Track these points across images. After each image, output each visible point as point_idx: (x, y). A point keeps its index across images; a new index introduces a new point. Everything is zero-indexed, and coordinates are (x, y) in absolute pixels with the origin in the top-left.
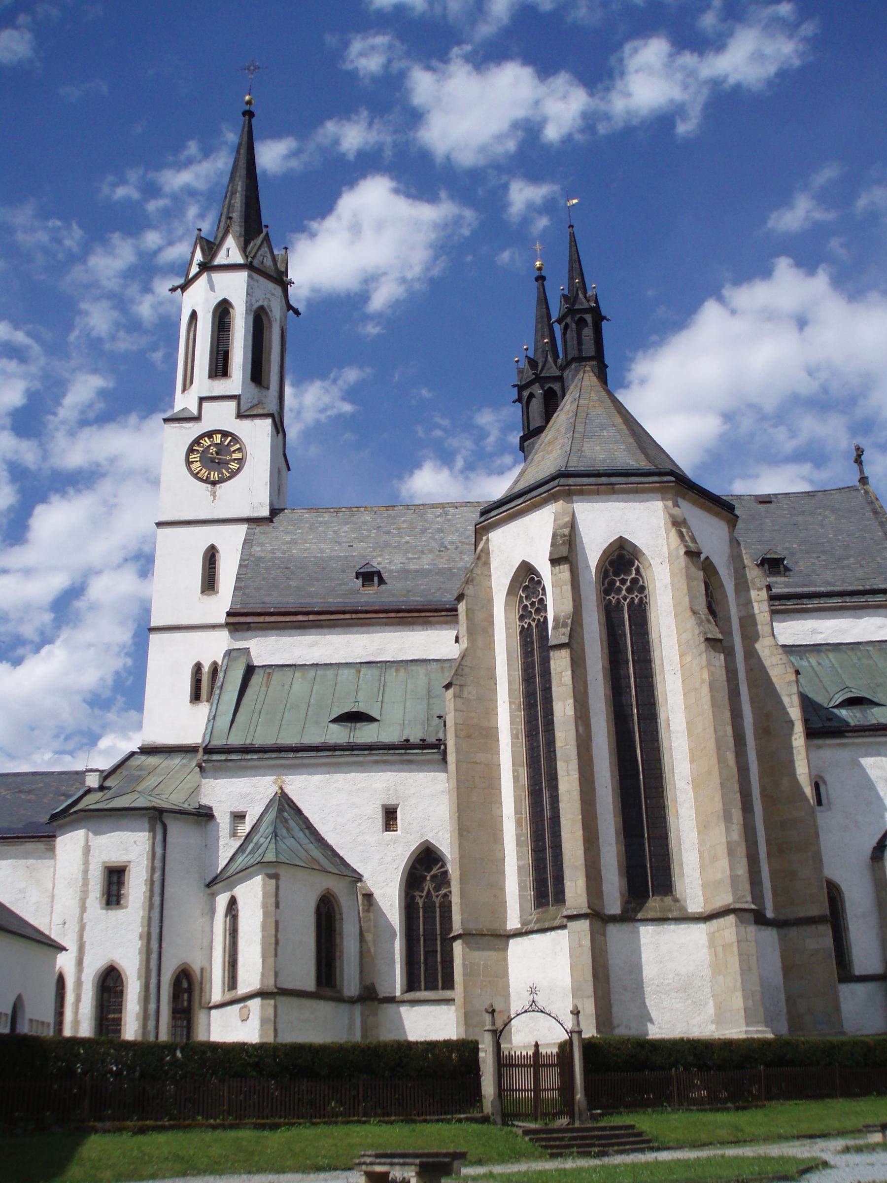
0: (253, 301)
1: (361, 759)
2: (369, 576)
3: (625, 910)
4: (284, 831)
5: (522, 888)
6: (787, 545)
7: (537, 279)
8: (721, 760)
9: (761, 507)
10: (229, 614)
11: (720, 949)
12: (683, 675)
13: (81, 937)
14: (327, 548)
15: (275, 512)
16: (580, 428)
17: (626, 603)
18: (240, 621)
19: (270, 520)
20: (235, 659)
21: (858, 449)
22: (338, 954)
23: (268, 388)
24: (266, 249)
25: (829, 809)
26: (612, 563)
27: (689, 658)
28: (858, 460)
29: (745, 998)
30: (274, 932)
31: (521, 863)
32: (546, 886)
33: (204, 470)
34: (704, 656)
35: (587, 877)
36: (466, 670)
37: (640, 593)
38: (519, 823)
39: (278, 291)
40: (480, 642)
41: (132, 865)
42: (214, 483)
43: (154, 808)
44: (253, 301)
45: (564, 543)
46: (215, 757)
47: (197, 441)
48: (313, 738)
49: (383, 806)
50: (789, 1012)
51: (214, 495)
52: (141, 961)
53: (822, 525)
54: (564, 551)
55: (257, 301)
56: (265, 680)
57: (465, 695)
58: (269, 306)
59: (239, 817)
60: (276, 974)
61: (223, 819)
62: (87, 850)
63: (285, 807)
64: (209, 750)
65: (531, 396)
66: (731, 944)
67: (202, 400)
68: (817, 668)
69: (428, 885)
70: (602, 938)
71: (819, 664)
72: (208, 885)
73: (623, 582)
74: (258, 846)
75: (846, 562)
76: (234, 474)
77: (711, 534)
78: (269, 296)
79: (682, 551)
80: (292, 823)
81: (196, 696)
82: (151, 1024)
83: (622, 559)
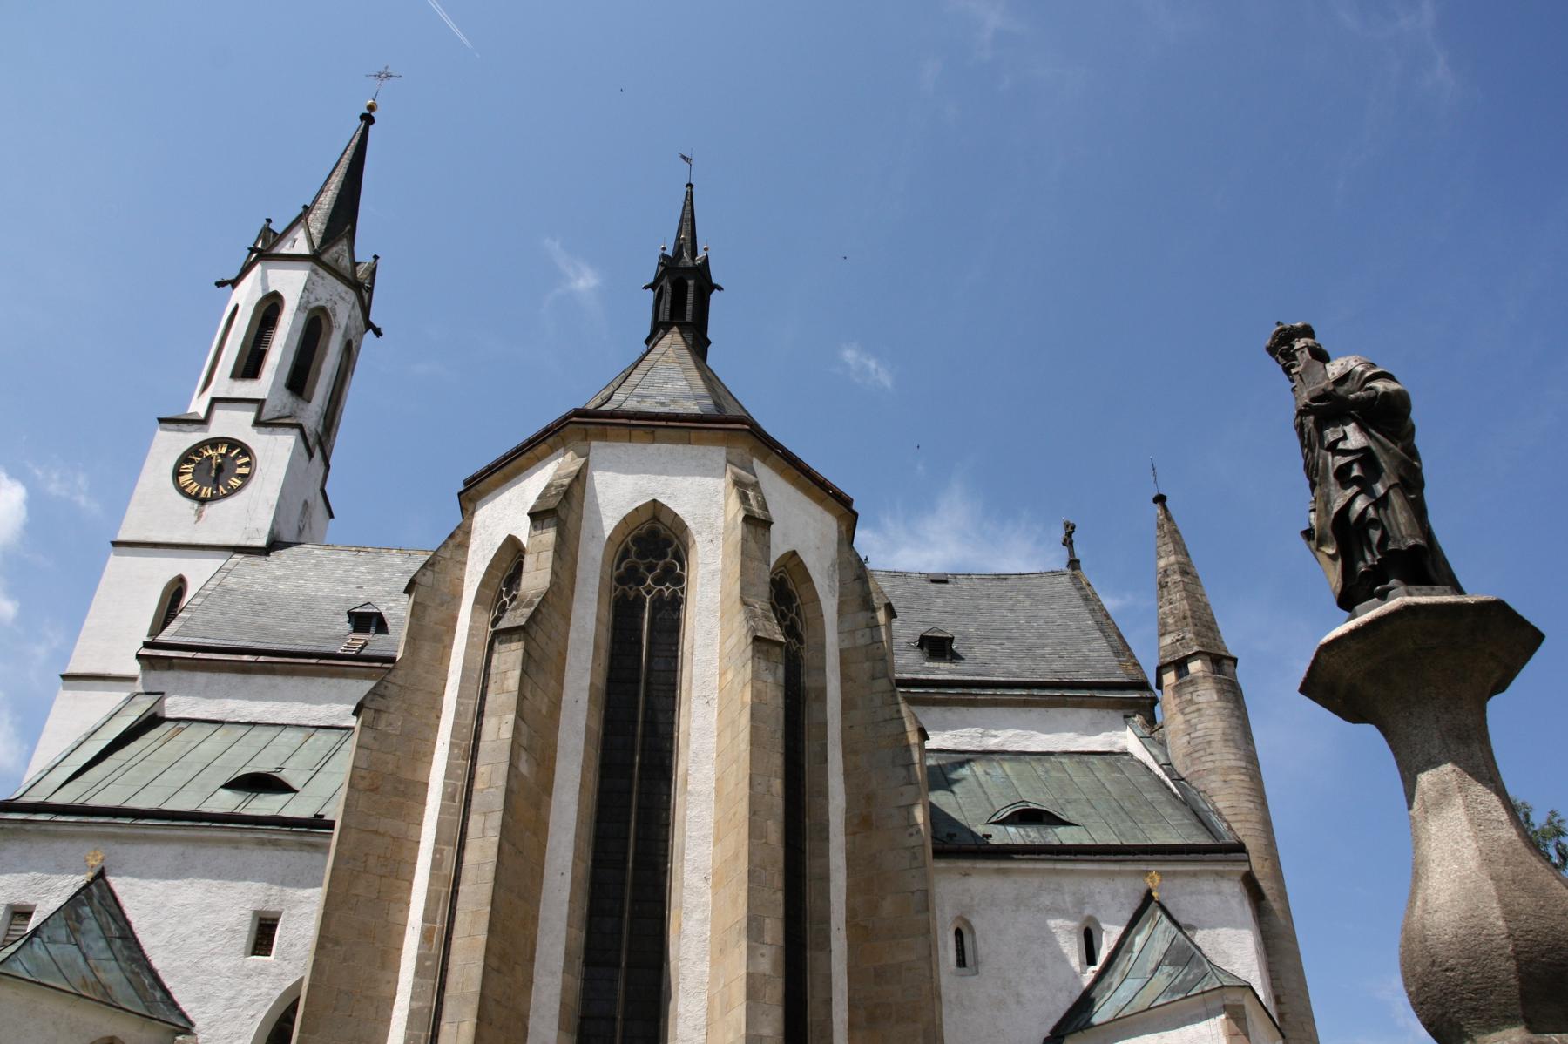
1: (236, 835)
4: (63, 933)
8: (755, 831)
9: (932, 586)
14: (326, 588)
15: (275, 544)
19: (265, 551)
26: (637, 540)
28: (1068, 542)
31: (416, 1005)
35: (479, 1018)
36: (393, 690)
39: (351, 296)
40: (426, 652)
42: (203, 501)
44: (312, 298)
47: (196, 449)
49: (256, 913)
51: (199, 515)
53: (1012, 610)
57: (382, 726)
58: (334, 310)
63: (96, 898)
67: (214, 401)
68: (983, 779)
73: (651, 569)
75: (1039, 652)
76: (233, 491)
80: (91, 925)
83: (655, 544)
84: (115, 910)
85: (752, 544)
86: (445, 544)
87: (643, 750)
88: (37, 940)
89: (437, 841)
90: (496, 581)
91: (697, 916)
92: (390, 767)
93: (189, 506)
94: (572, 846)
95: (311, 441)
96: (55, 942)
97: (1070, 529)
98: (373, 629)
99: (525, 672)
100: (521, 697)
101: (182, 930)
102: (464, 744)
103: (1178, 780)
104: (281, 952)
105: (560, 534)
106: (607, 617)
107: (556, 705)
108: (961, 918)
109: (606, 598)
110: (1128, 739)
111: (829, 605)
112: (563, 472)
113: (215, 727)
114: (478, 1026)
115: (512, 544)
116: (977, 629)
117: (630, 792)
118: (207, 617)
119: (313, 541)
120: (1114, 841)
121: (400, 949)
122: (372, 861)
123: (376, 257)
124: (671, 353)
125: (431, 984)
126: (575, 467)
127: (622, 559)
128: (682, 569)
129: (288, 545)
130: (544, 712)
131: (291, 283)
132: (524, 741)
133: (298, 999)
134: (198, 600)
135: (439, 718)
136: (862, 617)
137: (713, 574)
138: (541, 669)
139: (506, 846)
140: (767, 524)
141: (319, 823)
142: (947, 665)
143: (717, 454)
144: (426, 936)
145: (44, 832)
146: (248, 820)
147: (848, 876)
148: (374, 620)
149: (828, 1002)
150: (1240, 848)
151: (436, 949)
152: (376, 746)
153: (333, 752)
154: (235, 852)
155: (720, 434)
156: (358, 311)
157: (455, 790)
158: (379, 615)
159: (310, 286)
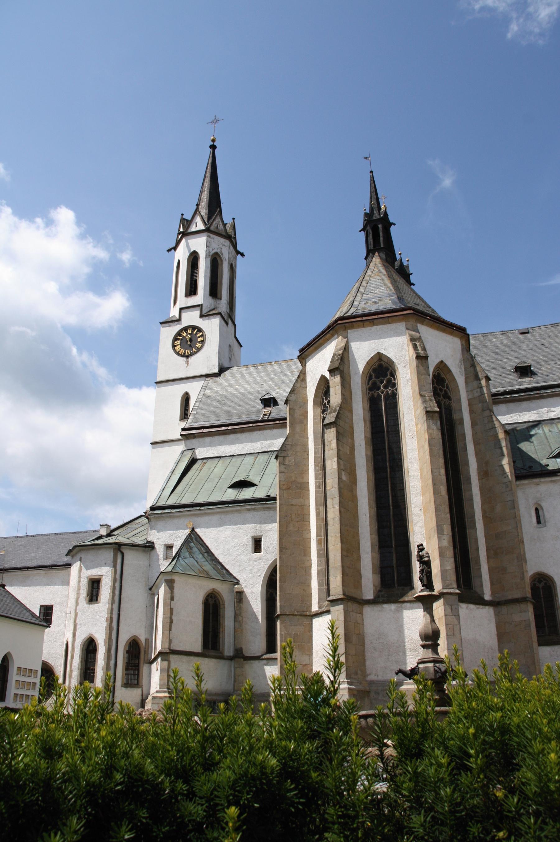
0: (211, 250)
4: (187, 554)
6: (535, 358)
9: (521, 336)
12: (417, 438)
14: (249, 388)
15: (222, 370)
17: (383, 395)
19: (218, 374)
22: (221, 629)
23: (221, 299)
24: (219, 220)
25: (545, 526)
26: (374, 370)
27: (419, 426)
30: (169, 615)
31: (319, 568)
33: (182, 349)
36: (288, 447)
37: (392, 388)
39: (227, 243)
41: (103, 578)
42: (188, 357)
44: (211, 250)
45: (338, 359)
47: (179, 333)
49: (252, 537)
51: (187, 363)
52: (106, 635)
55: (213, 250)
56: (200, 467)
57: (287, 462)
58: (221, 252)
59: (169, 547)
60: (170, 641)
61: (160, 550)
63: (193, 540)
66: (442, 617)
67: (181, 309)
68: (547, 434)
70: (361, 615)
71: (550, 431)
73: (382, 382)
76: (199, 350)
78: (221, 246)
80: (195, 549)
84: (201, 542)
85: (421, 368)
86: (297, 381)
87: (390, 460)
88: (180, 558)
89: (316, 505)
90: (321, 394)
91: (419, 525)
92: (293, 478)
93: (182, 360)
94: (367, 504)
95: (226, 318)
96: (186, 558)
98: (272, 405)
99: (338, 440)
100: (338, 450)
101: (227, 547)
102: (320, 465)
105: (342, 378)
106: (367, 406)
107: (352, 449)
108: (537, 503)
109: (365, 399)
111: (460, 380)
112: (339, 347)
113: (218, 459)
114: (343, 577)
115: (323, 378)
116: (544, 357)
117: (387, 478)
118: (203, 412)
119: (238, 365)
121: (310, 548)
122: (293, 516)
123: (234, 219)
124: (376, 270)
125: (324, 560)
126: (343, 344)
127: (369, 380)
128: (395, 380)
129: (227, 369)
130: (348, 453)
131: (199, 244)
132: (342, 467)
133: (276, 566)
134: (197, 404)
135: (308, 455)
136: (475, 383)
137: (407, 381)
139: (343, 510)
140: (426, 358)
141: (269, 499)
142: (529, 379)
143: (402, 326)
144: (319, 542)
145: (169, 516)
146: (242, 501)
147: (481, 497)
148: (272, 401)
149: (477, 549)
151: (323, 546)
152: (286, 471)
153: (267, 464)
154: (239, 515)
155: (401, 317)
156: (232, 248)
157: (320, 484)
158: (274, 398)
159: (209, 244)
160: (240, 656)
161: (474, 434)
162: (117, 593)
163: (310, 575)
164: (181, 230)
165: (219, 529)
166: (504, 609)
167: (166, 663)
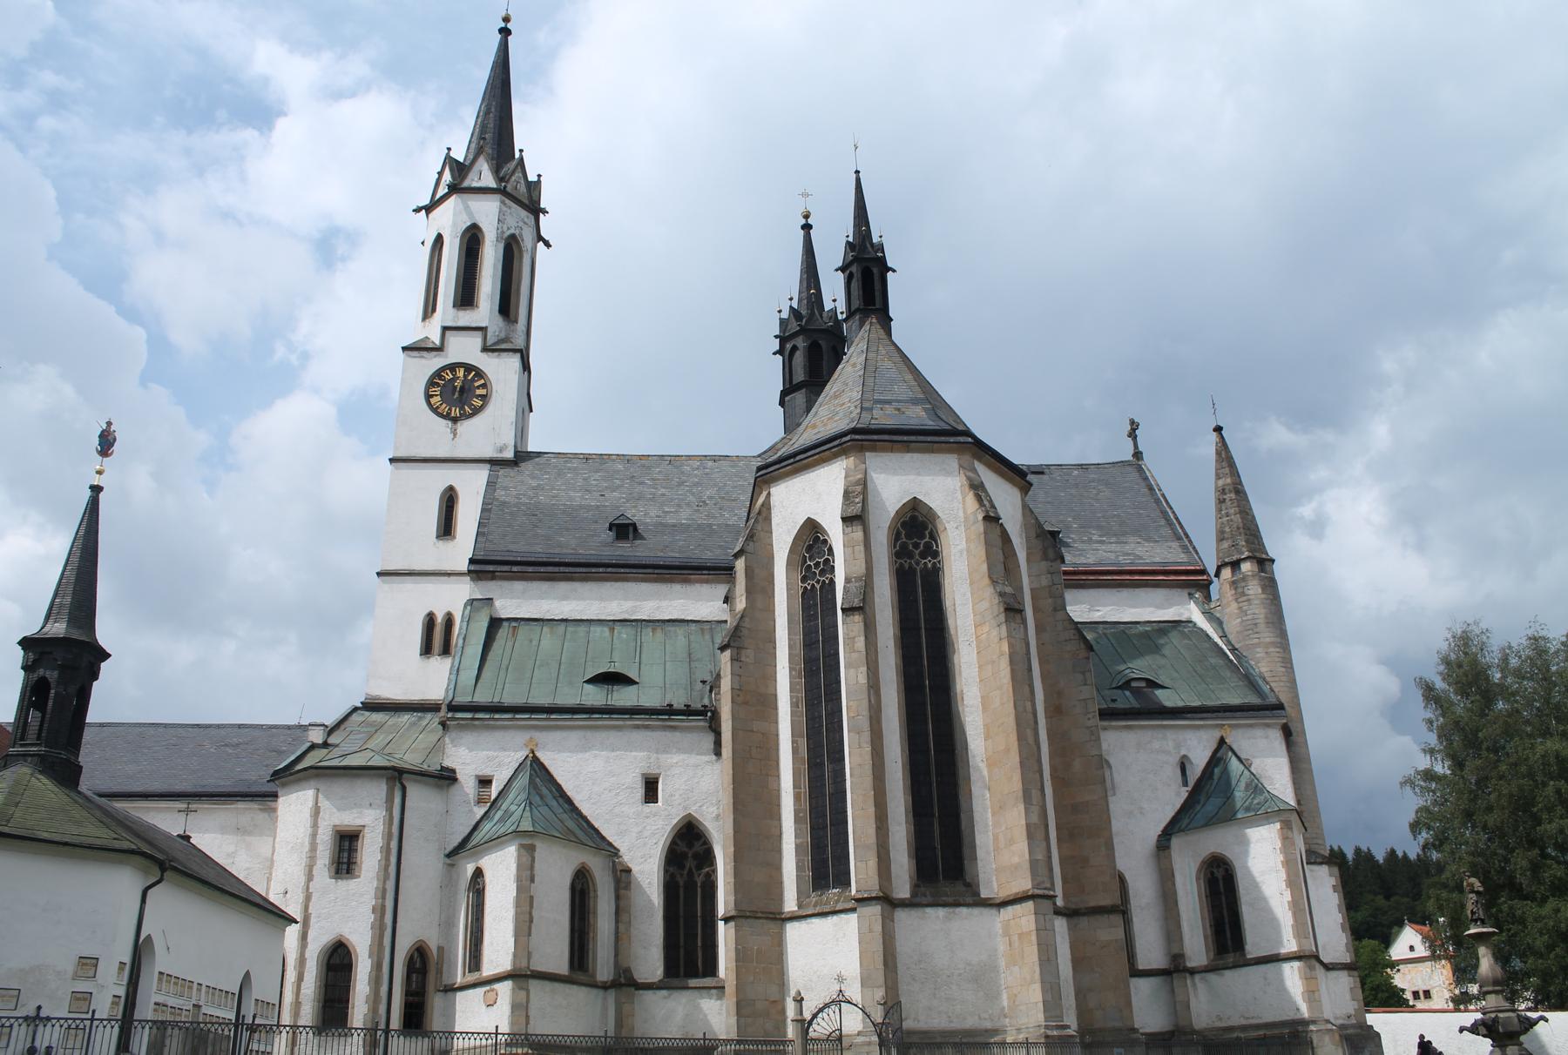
2: (624, 530)
3: (914, 894)
5: (799, 868)
7: (803, 227)
10: (472, 561)
11: (1015, 938)
13: (306, 908)
14: (577, 497)
16: (870, 382)
18: (483, 567)
20: (479, 610)
21: (1132, 422)
26: (904, 524)
28: (1133, 434)
29: (1044, 991)
32: (827, 867)
34: (1004, 627)
36: (745, 632)
38: (797, 797)
42: (455, 420)
43: (394, 768)
46: (459, 715)
47: (438, 374)
48: (567, 698)
50: (1078, 1006)
54: (855, 509)
59: (485, 782)
61: (468, 784)
62: (316, 811)
63: (537, 770)
64: (452, 708)
65: (795, 348)
67: (445, 329)
69: (690, 863)
72: (448, 856)
74: (508, 815)
76: (476, 411)
77: (1006, 498)
79: (980, 517)
80: (545, 791)
81: (427, 650)
82: (382, 1009)
83: (916, 527)
97: (1134, 426)
103: (1233, 650)
104: (665, 802)
110: (1193, 612)
120: (1196, 703)
127: (896, 540)
137: (961, 552)
138: (870, 629)
143: (952, 461)
150: (1280, 707)
160: (625, 983)
161: (1040, 645)
162: (393, 860)
163: (779, 851)
164: (447, 177)
165: (580, 755)
166: (1084, 922)
167: (523, 993)
